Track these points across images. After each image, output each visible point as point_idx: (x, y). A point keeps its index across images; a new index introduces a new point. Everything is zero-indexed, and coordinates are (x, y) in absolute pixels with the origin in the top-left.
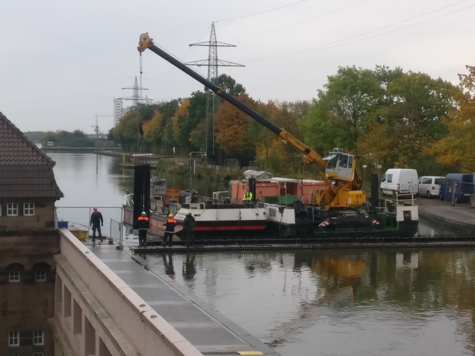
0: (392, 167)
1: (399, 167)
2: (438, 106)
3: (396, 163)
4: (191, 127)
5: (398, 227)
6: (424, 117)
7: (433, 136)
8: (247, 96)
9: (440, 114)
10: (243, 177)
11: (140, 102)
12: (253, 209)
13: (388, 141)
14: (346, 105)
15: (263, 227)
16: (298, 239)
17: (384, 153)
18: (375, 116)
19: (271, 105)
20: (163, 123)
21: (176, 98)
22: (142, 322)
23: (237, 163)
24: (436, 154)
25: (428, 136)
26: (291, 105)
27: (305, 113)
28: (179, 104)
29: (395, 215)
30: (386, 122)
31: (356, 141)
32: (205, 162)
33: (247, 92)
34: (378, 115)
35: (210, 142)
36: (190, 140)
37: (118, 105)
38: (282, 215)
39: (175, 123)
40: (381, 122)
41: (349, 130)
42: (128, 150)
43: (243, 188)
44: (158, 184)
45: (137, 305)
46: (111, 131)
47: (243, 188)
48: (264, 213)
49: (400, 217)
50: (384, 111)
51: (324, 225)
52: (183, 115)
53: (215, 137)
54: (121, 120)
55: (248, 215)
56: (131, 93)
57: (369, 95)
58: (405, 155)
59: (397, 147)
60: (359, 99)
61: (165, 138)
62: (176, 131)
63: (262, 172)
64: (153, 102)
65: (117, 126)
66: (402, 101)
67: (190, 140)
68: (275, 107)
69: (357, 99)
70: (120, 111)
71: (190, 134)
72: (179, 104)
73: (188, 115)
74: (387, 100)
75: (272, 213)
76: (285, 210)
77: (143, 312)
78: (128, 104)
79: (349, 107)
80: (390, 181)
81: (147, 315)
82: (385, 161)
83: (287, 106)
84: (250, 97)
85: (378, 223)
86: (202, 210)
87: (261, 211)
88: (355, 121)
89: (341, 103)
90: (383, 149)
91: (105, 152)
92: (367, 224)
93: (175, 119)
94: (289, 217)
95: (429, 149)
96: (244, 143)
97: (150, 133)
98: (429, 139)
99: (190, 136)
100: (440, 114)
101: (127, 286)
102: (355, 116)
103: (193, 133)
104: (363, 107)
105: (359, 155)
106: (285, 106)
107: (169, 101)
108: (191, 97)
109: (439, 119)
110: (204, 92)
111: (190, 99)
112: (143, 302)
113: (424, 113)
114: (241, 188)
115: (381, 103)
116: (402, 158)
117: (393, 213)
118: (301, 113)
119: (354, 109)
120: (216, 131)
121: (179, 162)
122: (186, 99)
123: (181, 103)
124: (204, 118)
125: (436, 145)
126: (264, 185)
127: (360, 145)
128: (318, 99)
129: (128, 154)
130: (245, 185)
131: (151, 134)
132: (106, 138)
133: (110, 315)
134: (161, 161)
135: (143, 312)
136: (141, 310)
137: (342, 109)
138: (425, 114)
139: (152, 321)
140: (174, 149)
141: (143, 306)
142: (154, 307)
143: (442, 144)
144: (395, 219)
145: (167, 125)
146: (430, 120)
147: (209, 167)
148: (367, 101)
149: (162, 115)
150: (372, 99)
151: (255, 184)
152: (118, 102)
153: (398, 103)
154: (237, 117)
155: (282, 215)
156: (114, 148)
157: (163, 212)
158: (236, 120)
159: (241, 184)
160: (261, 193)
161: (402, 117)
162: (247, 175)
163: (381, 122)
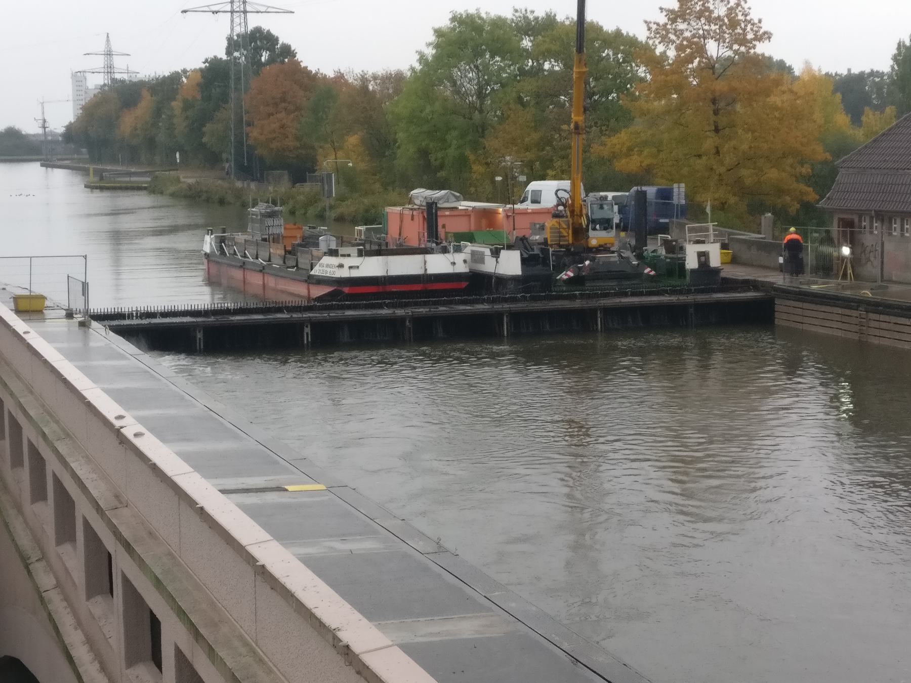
0: (543, 178)
1: (555, 178)
2: (617, 76)
3: (550, 172)
4: (204, 118)
5: (688, 278)
6: (594, 94)
7: (608, 126)
8: (298, 63)
9: (621, 89)
10: (410, 201)
11: (118, 76)
12: (446, 255)
13: (535, 136)
14: (466, 76)
15: (464, 284)
16: (387, 301)
17: (529, 156)
18: (514, 95)
19: (340, 77)
20: (157, 113)
21: (179, 69)
22: (120, 443)
23: (286, 177)
24: (614, 156)
25: (601, 126)
26: (375, 78)
27: (397, 91)
28: (184, 79)
29: (683, 260)
30: (533, 103)
31: (483, 137)
32: (232, 176)
33: (299, 57)
34: (519, 92)
35: (240, 143)
36: (205, 140)
37: (78, 83)
38: (497, 262)
39: (177, 112)
40: (523, 105)
41: (471, 119)
42: (99, 160)
43: (412, 219)
44: (270, 217)
45: (111, 417)
46: (69, 128)
47: (412, 219)
48: (465, 261)
49: (692, 263)
50: (529, 85)
51: (565, 277)
52: (190, 98)
53: (247, 134)
54: (84, 108)
55: (439, 264)
56: (99, 62)
57: (503, 59)
58: (717, 148)
59: (551, 145)
60: (486, 66)
61: (161, 137)
62: (181, 125)
63: (443, 192)
64: (138, 75)
65: (78, 119)
66: (557, 68)
67: (205, 140)
68: (346, 81)
69: (483, 67)
70: (83, 93)
71: (204, 129)
72: (184, 79)
73: (199, 97)
74: (532, 67)
75: (477, 258)
76: (504, 253)
77: (122, 427)
78: (96, 81)
79: (470, 80)
80: (536, 201)
81: (128, 432)
82: (532, 170)
83: (367, 80)
84: (303, 65)
85: (653, 273)
86: (361, 259)
87: (459, 258)
88: (481, 104)
89: (456, 73)
90: (527, 149)
91: (59, 163)
92: (637, 274)
93: (177, 105)
94: (510, 264)
95: (602, 148)
96: (298, 144)
97: (136, 129)
98: (601, 131)
99: (203, 134)
100: (621, 89)
101: (94, 385)
102: (481, 95)
103: (208, 127)
104: (494, 78)
105: (489, 160)
106: (364, 80)
107: (167, 74)
108: (203, 66)
109: (618, 96)
110: (225, 57)
111: (201, 70)
112: (122, 412)
113: (594, 87)
114: (407, 219)
115: (522, 72)
116: (559, 163)
117: (679, 256)
118: (391, 91)
119: (478, 83)
120: (249, 124)
121: (187, 177)
122: (195, 71)
123: (186, 77)
124: (226, 102)
125: (614, 140)
126: (447, 213)
127: (491, 143)
128: (418, 67)
129: (100, 167)
130: (415, 213)
131: (138, 132)
132: (60, 139)
133: (68, 435)
134: (157, 177)
135: (122, 427)
136: (117, 424)
137: (459, 83)
138: (595, 89)
139: (137, 442)
140: (178, 155)
141: (120, 417)
142: (141, 420)
143: (621, 139)
144: (682, 266)
145: (163, 116)
146: (604, 99)
147: (239, 184)
148: (501, 69)
149: (154, 98)
150: (509, 66)
151: (436, 212)
152: (78, 78)
153: (551, 71)
154: (283, 100)
155: (497, 262)
156: (76, 156)
157: (284, 262)
158: (283, 105)
159: (406, 212)
160: (444, 226)
161: (558, 96)
162: (417, 197)
163: (523, 105)
